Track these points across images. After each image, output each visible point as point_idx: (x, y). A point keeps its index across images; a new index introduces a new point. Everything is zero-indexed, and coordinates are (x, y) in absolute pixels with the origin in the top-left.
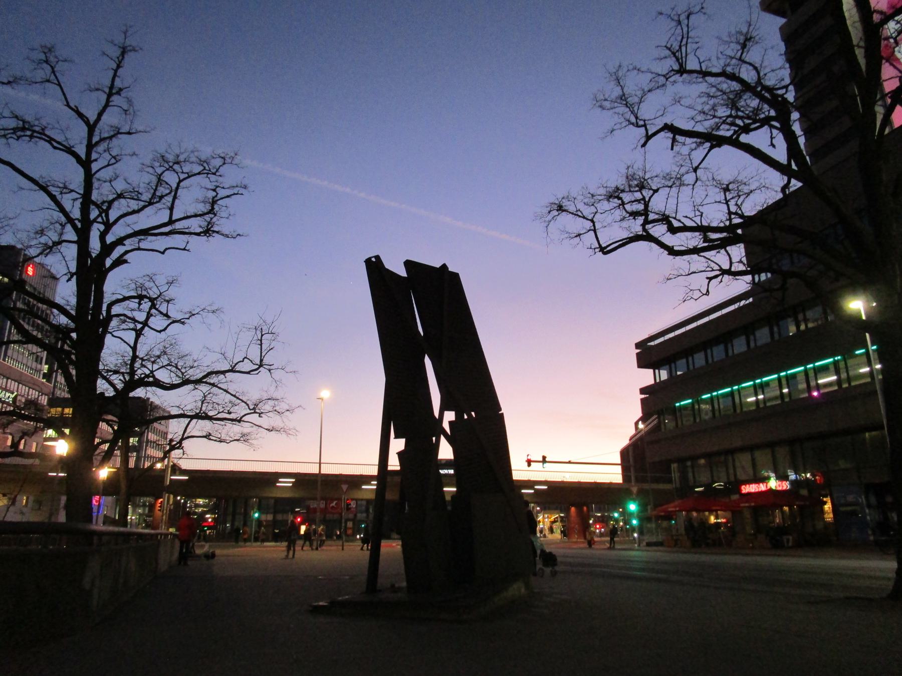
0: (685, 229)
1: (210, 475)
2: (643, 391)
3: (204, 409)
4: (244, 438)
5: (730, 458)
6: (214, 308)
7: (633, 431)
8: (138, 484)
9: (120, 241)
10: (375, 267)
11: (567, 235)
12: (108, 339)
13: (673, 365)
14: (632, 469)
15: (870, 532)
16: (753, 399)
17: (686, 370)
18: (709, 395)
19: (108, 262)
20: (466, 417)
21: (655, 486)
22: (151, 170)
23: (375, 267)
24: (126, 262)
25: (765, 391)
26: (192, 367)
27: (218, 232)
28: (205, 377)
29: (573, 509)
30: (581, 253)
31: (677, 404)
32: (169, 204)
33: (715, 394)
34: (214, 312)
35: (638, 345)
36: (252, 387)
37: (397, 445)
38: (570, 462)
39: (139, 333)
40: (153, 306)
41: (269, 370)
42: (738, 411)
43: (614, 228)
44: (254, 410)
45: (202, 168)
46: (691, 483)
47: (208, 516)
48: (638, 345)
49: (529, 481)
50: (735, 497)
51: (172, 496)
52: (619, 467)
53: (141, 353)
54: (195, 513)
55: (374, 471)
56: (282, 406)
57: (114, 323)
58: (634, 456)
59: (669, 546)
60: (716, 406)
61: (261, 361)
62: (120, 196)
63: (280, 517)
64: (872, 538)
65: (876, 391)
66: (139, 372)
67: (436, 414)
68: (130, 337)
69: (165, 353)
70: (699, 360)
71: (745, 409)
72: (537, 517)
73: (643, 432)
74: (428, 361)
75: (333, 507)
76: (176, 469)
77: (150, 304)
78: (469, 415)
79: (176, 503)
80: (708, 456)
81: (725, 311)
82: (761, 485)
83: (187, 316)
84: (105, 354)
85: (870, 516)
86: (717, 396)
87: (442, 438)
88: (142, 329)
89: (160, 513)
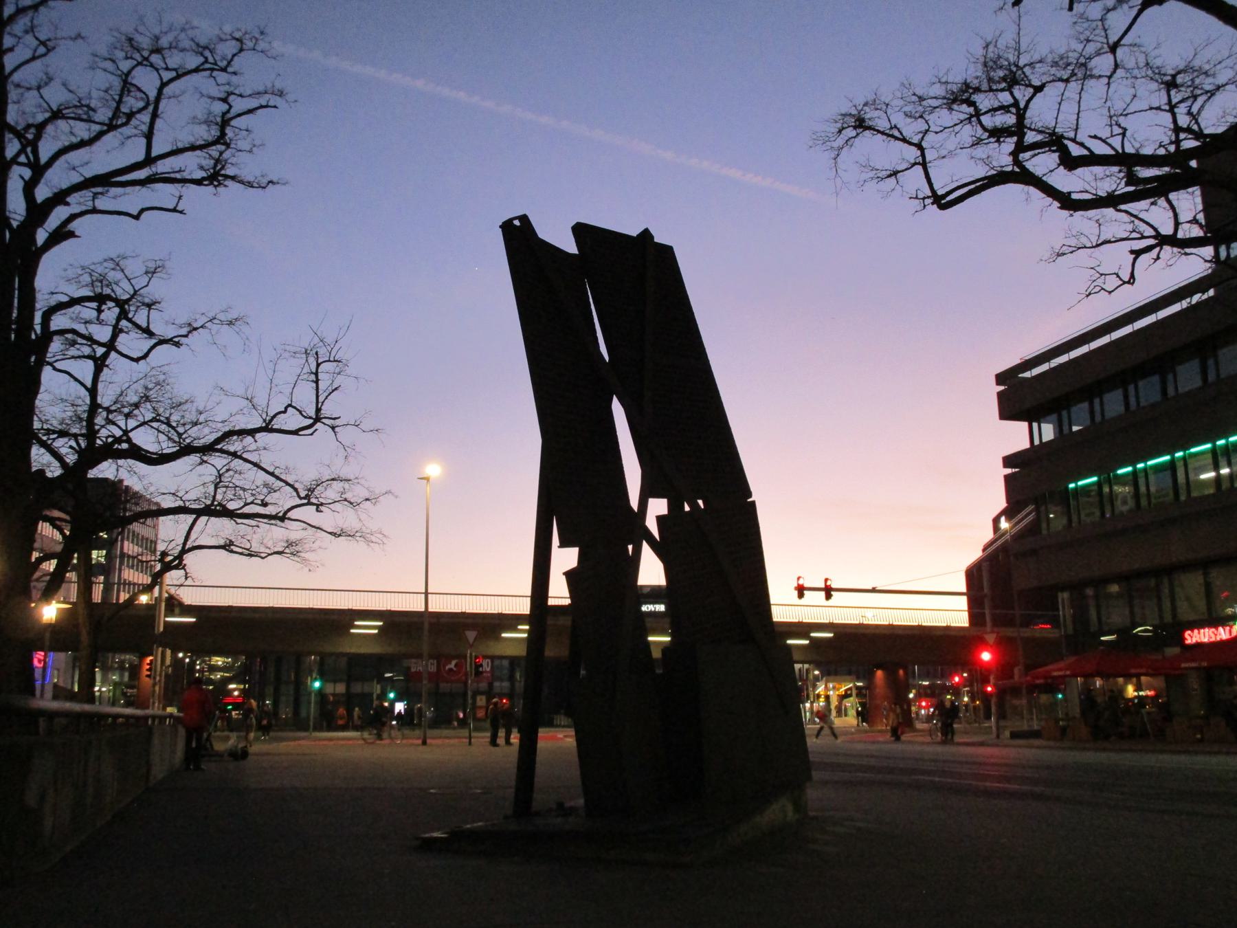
2: (1008, 461)
3: (219, 497)
4: (290, 549)
5: (1166, 581)
6: (230, 316)
7: (989, 535)
8: (111, 631)
9: (60, 198)
10: (519, 237)
11: (872, 174)
12: (47, 374)
14: (987, 603)
18: (1130, 469)
19: (41, 236)
20: (687, 508)
22: (109, 65)
23: (519, 237)
24: (72, 235)
26: (195, 424)
27: (233, 178)
28: (218, 441)
30: (900, 207)
31: (1072, 486)
32: (145, 128)
33: (1140, 466)
34: (231, 323)
35: (1001, 378)
37: (565, 559)
38: (874, 590)
39: (100, 364)
40: (123, 315)
41: (333, 428)
43: (960, 157)
44: (308, 498)
45: (202, 59)
47: (232, 686)
48: (1001, 378)
49: (800, 624)
51: (169, 652)
52: (965, 598)
53: (105, 399)
54: (211, 682)
57: (56, 346)
58: (989, 580)
60: (1143, 489)
62: (57, 115)
63: (357, 688)
67: (634, 503)
68: (85, 370)
69: (147, 398)
70: (1113, 403)
72: (815, 687)
73: (1008, 536)
75: (451, 670)
76: (174, 604)
77: (117, 310)
78: (694, 505)
79: (177, 663)
83: (184, 331)
86: (1145, 470)
87: (646, 549)
88: (106, 356)
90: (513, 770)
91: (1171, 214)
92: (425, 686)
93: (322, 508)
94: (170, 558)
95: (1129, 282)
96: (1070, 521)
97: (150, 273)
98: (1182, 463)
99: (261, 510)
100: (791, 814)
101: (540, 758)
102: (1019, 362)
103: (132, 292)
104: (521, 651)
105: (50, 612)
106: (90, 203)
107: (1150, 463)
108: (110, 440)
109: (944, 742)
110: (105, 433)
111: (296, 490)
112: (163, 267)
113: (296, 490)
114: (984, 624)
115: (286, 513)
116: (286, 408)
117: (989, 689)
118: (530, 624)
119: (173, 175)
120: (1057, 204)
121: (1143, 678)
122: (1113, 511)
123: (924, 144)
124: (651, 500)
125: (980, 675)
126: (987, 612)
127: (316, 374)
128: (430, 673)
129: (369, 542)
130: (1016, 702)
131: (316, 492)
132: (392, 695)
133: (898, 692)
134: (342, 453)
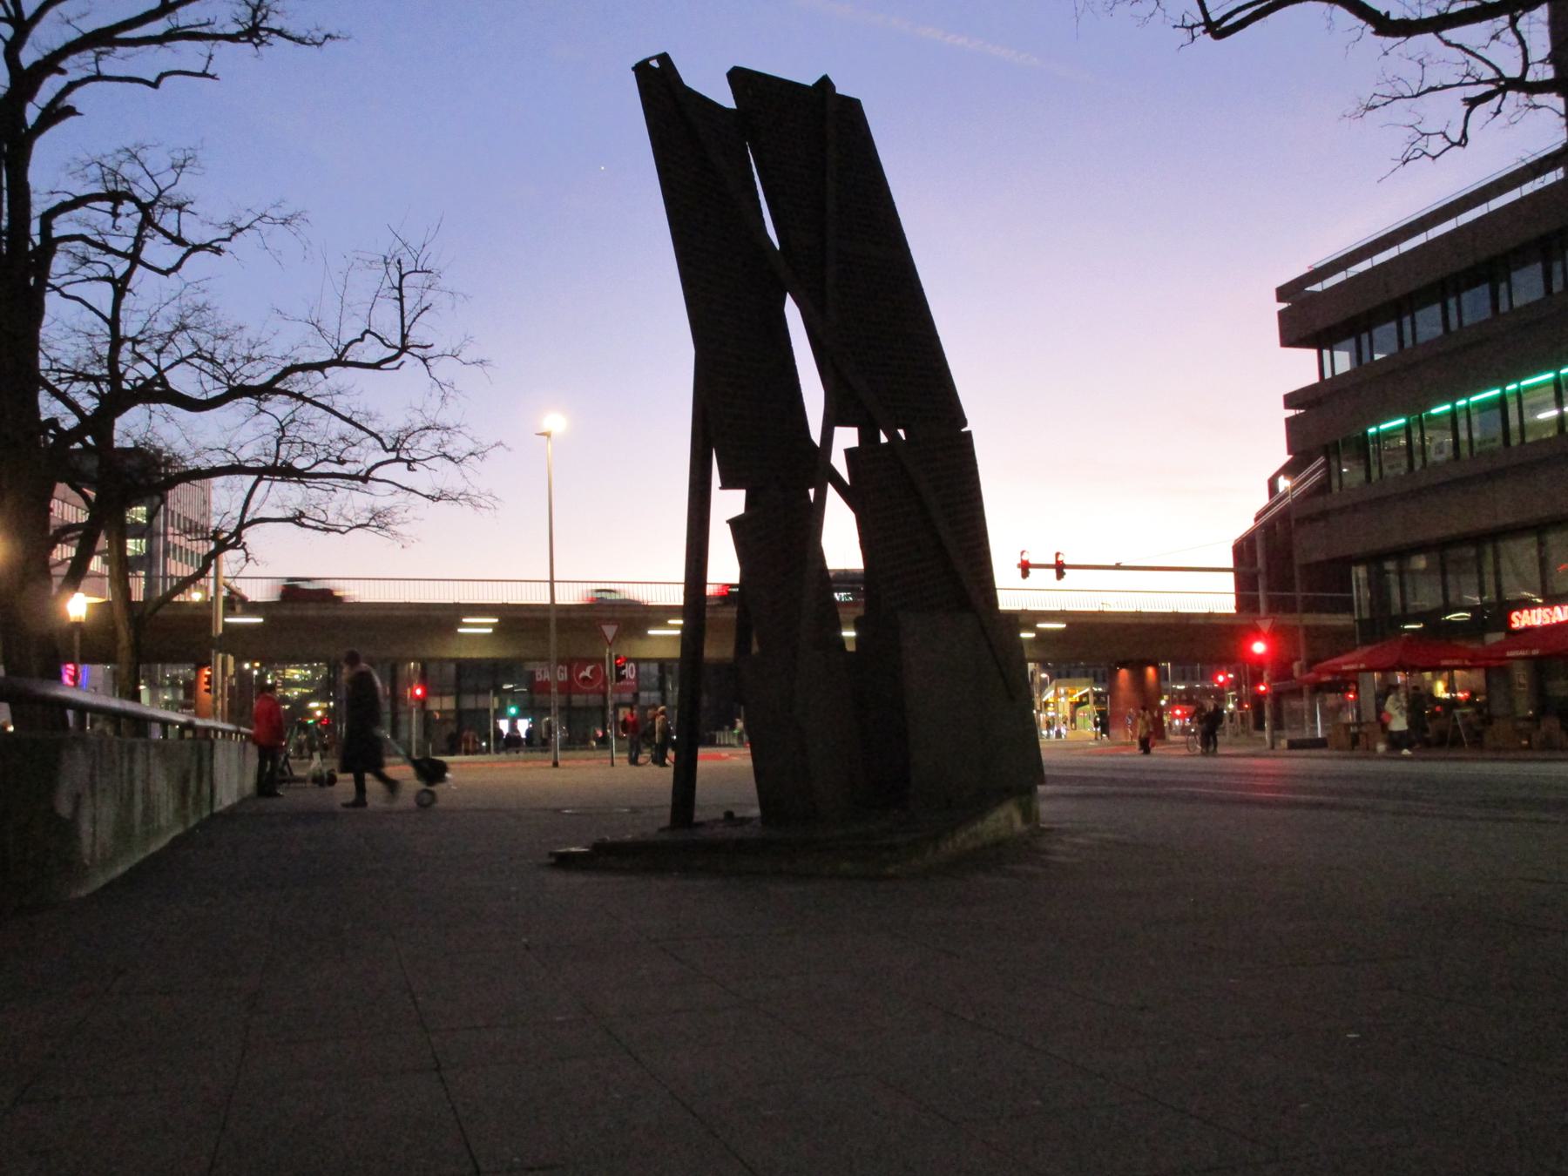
1: (382, 613)
2: (1291, 400)
3: (283, 453)
4: (378, 520)
5: (1489, 550)
6: (286, 211)
7: (1263, 500)
8: (157, 634)
9: (50, 64)
10: (658, 83)
12: (51, 300)
13: (1365, 338)
14: (1261, 583)
17: (1394, 348)
18: (1447, 407)
19: (32, 113)
20: (884, 439)
21: (1310, 619)
23: (658, 83)
24: (71, 111)
26: (249, 359)
27: (280, 33)
28: (277, 379)
29: (1124, 674)
31: (1372, 430)
33: (1461, 403)
34: (285, 222)
35: (1283, 293)
36: (388, 399)
37: (728, 503)
38: (1118, 567)
39: (121, 287)
41: (424, 360)
42: (1515, 442)
44: (397, 449)
46: (1396, 607)
47: (313, 705)
48: (1283, 293)
50: (1494, 638)
51: (231, 659)
52: (1231, 576)
53: (129, 328)
54: (285, 700)
55: (676, 597)
57: (60, 264)
58: (1265, 558)
59: (1338, 748)
60: (1463, 435)
66: (131, 375)
67: (816, 436)
68: (102, 295)
69: (183, 327)
70: (1428, 324)
71: (1529, 439)
72: (1041, 692)
73: (1288, 500)
74: (778, 246)
75: (585, 678)
76: (235, 602)
77: (139, 216)
78: (893, 436)
79: (242, 676)
80: (1439, 548)
81: (1496, 204)
82: (1557, 609)
83: (225, 234)
84: (49, 331)
86: (1467, 408)
87: (832, 494)
88: (128, 275)
89: (208, 697)
90: (668, 799)
91: (1519, 50)
92: (556, 700)
93: (414, 465)
94: (225, 535)
95: (1459, 144)
96: (1368, 477)
97: (179, 167)
98: (1514, 399)
99: (336, 469)
100: (1019, 825)
101: (701, 777)
102: (1306, 271)
103: (155, 192)
104: (674, 652)
105: (78, 606)
106: (93, 67)
107: (1474, 399)
108: (140, 382)
109: (1205, 754)
110: (135, 372)
111: (380, 440)
112: (194, 158)
113: (380, 440)
114: (1256, 610)
115: (369, 471)
117: (1262, 688)
118: (684, 617)
119: (199, 30)
120: (1371, 29)
121: (1456, 672)
122: (1424, 460)
124: (837, 429)
125: (1254, 672)
126: (1261, 595)
127: (400, 289)
129: (477, 506)
130: (1295, 704)
131: (406, 445)
132: (513, 711)
133: (1147, 701)
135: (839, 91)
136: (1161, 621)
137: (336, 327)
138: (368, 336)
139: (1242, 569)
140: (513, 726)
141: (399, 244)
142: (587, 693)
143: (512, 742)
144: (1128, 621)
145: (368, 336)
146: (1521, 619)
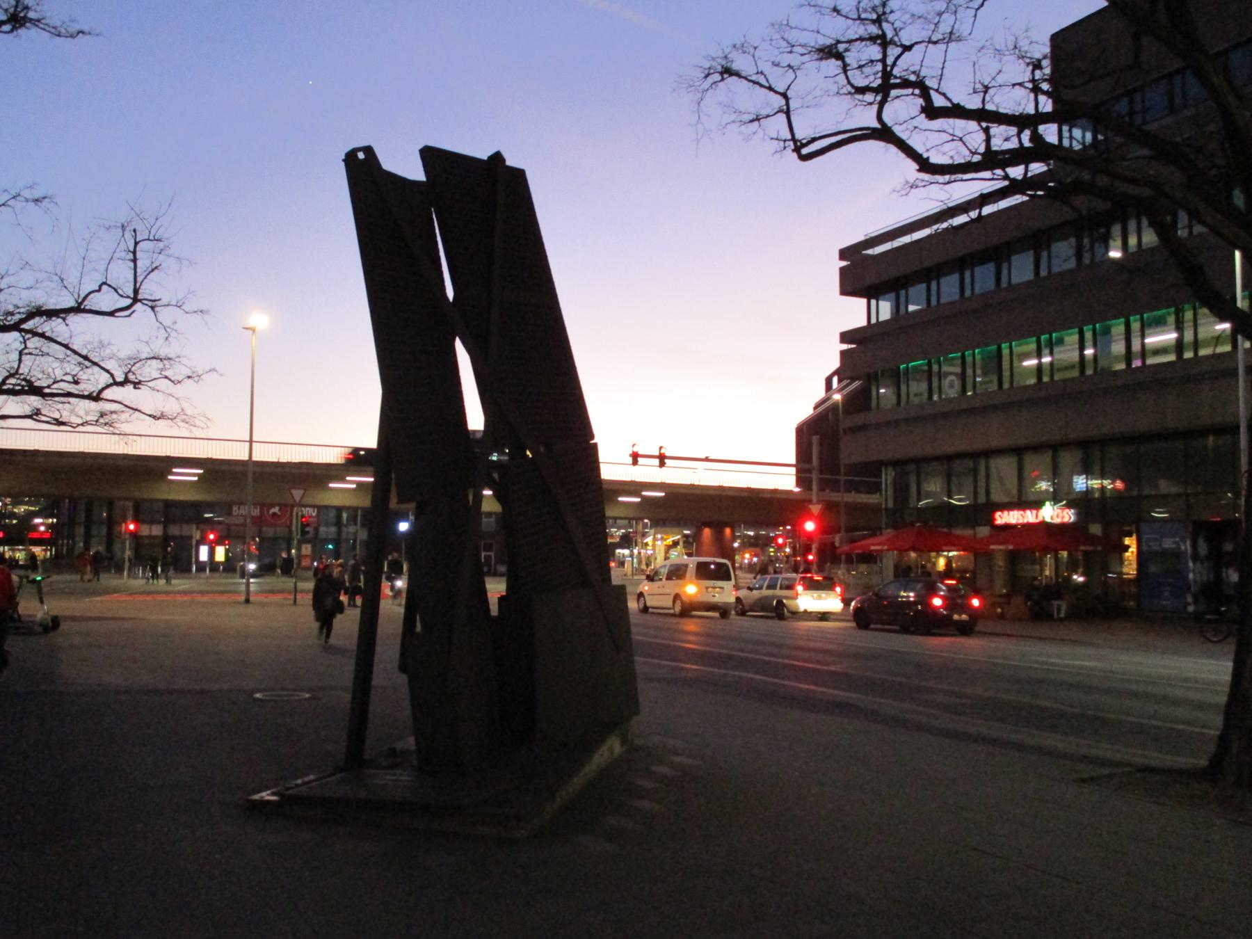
0: (957, 111)
2: (845, 337)
6: (38, 194)
7: (821, 394)
10: (363, 170)
11: (733, 117)
15: (1190, 599)
16: (1032, 362)
17: (925, 306)
21: (850, 497)
23: (363, 170)
25: (1056, 350)
29: (707, 532)
30: (764, 152)
34: (37, 201)
35: (844, 254)
36: (117, 339)
38: (707, 459)
41: (153, 308)
43: (828, 106)
47: (38, 521)
48: (844, 254)
49: (633, 483)
50: (983, 531)
54: (13, 515)
56: (176, 371)
58: (819, 438)
61: (136, 291)
63: (174, 530)
64: (1191, 609)
65: (1236, 369)
70: (949, 287)
74: (458, 345)
75: (274, 514)
82: (1028, 512)
85: (1195, 573)
116: (100, 287)
123: (789, 94)
127: (134, 253)
128: (253, 517)
134: (163, 334)
135: (508, 163)
136: (737, 494)
137: (76, 281)
138: (105, 288)
139: (802, 465)
140: (212, 553)
141: (133, 214)
142: (276, 526)
143: (213, 565)
144: (711, 492)
145: (105, 288)
146: (1006, 518)
